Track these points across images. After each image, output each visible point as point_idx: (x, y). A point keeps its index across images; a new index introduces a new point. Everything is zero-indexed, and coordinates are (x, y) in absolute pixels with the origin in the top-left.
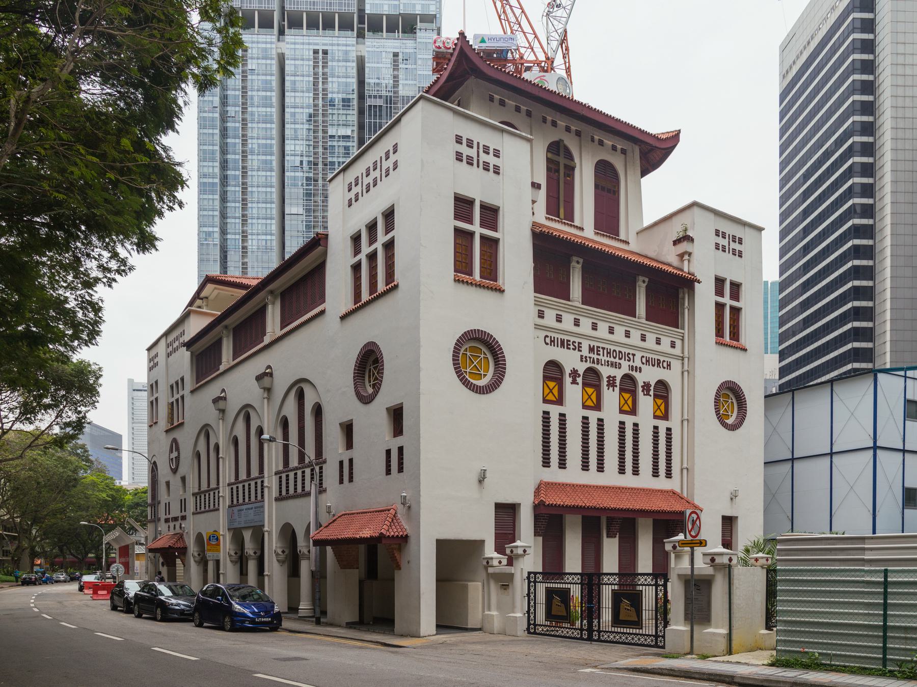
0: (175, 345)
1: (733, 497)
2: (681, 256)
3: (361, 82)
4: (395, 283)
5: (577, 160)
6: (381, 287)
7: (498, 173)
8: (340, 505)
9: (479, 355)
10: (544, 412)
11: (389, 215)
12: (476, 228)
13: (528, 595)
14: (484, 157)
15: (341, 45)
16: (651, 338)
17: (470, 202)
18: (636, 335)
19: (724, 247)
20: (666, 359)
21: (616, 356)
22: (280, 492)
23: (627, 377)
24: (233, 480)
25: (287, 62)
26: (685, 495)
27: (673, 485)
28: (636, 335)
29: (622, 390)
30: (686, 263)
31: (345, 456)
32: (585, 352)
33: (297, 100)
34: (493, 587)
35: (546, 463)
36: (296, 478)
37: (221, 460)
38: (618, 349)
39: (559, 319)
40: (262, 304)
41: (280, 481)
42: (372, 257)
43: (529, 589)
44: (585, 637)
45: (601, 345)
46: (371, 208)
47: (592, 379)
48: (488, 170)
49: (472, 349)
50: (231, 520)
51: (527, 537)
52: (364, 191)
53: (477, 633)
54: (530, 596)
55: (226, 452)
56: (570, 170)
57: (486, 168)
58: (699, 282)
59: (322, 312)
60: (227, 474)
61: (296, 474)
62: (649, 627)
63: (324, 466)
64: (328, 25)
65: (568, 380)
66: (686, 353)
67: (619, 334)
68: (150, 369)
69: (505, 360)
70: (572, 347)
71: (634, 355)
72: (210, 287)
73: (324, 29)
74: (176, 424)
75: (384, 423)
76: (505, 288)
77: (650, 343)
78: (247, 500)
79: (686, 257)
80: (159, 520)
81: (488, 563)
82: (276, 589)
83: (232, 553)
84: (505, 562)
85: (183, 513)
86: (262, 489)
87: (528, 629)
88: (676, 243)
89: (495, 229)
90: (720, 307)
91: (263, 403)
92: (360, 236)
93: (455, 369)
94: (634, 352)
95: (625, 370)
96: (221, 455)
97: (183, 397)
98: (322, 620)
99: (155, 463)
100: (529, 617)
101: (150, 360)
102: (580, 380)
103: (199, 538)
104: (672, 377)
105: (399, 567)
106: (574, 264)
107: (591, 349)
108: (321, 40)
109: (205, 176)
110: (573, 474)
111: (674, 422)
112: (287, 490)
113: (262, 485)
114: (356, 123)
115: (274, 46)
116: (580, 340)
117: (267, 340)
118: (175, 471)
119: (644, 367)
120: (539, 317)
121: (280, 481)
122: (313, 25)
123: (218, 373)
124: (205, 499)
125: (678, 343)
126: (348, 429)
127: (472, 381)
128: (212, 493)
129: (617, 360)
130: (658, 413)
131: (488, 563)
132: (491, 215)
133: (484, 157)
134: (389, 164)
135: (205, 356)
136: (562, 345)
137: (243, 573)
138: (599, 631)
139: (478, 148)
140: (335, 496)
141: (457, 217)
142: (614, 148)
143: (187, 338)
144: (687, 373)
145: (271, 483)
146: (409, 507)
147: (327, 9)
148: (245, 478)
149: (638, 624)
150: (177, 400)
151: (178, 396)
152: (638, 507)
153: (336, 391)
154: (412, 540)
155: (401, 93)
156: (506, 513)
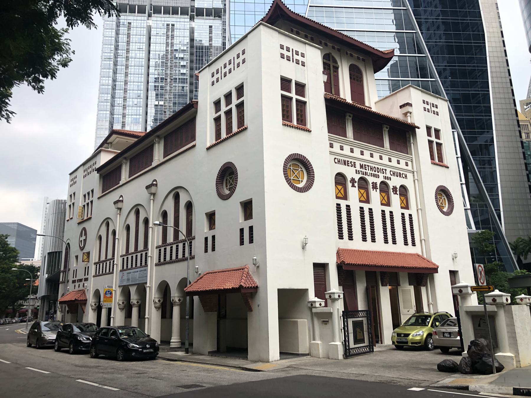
0: (89, 171)
1: (454, 258)
2: (405, 114)
4: (245, 126)
5: (339, 63)
6: (235, 129)
7: (304, 66)
8: (212, 266)
9: (298, 167)
10: (337, 204)
11: (240, 89)
12: (293, 95)
13: (344, 328)
15: (182, 23)
17: (290, 81)
18: (385, 158)
19: (428, 109)
20: (404, 173)
21: (377, 171)
24: (124, 253)
25: (152, 29)
26: (425, 256)
27: (416, 250)
28: (385, 158)
30: (409, 118)
32: (358, 168)
35: (341, 237)
36: (141, 257)
37: (117, 241)
38: (376, 166)
39: (342, 148)
40: (152, 143)
41: (123, 261)
42: (228, 113)
46: (229, 84)
47: (363, 184)
48: (299, 64)
50: (122, 280)
51: (334, 287)
53: (305, 357)
55: (121, 236)
56: (336, 68)
57: (297, 62)
58: (418, 128)
59: (194, 146)
60: (121, 249)
63: (193, 241)
66: (415, 169)
67: (376, 158)
68: (71, 186)
69: (313, 172)
70: (350, 165)
71: (386, 170)
72: (114, 136)
74: (85, 218)
77: (394, 163)
79: (409, 114)
80: (68, 281)
81: (312, 305)
82: (153, 329)
83: (121, 303)
84: (323, 304)
85: (86, 277)
89: (303, 96)
90: (430, 142)
91: (150, 202)
92: (231, 93)
93: (285, 177)
94: (386, 168)
95: (381, 179)
96: (117, 237)
97: (92, 202)
98: (189, 350)
99: (68, 244)
102: (356, 185)
103: (97, 294)
104: (408, 183)
105: (251, 310)
106: (347, 117)
107: (361, 166)
108: (171, 19)
110: (357, 244)
112: (106, 271)
113: (146, 256)
114: (189, 59)
115: (145, 22)
116: (355, 161)
117: (154, 164)
118: (82, 249)
119: (392, 177)
120: (330, 147)
121: (123, 261)
122: (167, 11)
123: (118, 185)
124: (104, 267)
126: (211, 217)
127: (296, 185)
128: (108, 262)
129: (376, 173)
130: (403, 205)
131: (312, 305)
132: (301, 88)
134: (240, 60)
136: (345, 164)
137: (129, 315)
139: (293, 52)
140: (202, 262)
141: (282, 89)
142: (358, 58)
143: (98, 166)
145: (153, 254)
146: (258, 267)
147: (174, 5)
148: (142, 249)
150: (88, 204)
152: (400, 265)
153: (203, 193)
154: (261, 290)
155: (213, 45)
156: (320, 269)
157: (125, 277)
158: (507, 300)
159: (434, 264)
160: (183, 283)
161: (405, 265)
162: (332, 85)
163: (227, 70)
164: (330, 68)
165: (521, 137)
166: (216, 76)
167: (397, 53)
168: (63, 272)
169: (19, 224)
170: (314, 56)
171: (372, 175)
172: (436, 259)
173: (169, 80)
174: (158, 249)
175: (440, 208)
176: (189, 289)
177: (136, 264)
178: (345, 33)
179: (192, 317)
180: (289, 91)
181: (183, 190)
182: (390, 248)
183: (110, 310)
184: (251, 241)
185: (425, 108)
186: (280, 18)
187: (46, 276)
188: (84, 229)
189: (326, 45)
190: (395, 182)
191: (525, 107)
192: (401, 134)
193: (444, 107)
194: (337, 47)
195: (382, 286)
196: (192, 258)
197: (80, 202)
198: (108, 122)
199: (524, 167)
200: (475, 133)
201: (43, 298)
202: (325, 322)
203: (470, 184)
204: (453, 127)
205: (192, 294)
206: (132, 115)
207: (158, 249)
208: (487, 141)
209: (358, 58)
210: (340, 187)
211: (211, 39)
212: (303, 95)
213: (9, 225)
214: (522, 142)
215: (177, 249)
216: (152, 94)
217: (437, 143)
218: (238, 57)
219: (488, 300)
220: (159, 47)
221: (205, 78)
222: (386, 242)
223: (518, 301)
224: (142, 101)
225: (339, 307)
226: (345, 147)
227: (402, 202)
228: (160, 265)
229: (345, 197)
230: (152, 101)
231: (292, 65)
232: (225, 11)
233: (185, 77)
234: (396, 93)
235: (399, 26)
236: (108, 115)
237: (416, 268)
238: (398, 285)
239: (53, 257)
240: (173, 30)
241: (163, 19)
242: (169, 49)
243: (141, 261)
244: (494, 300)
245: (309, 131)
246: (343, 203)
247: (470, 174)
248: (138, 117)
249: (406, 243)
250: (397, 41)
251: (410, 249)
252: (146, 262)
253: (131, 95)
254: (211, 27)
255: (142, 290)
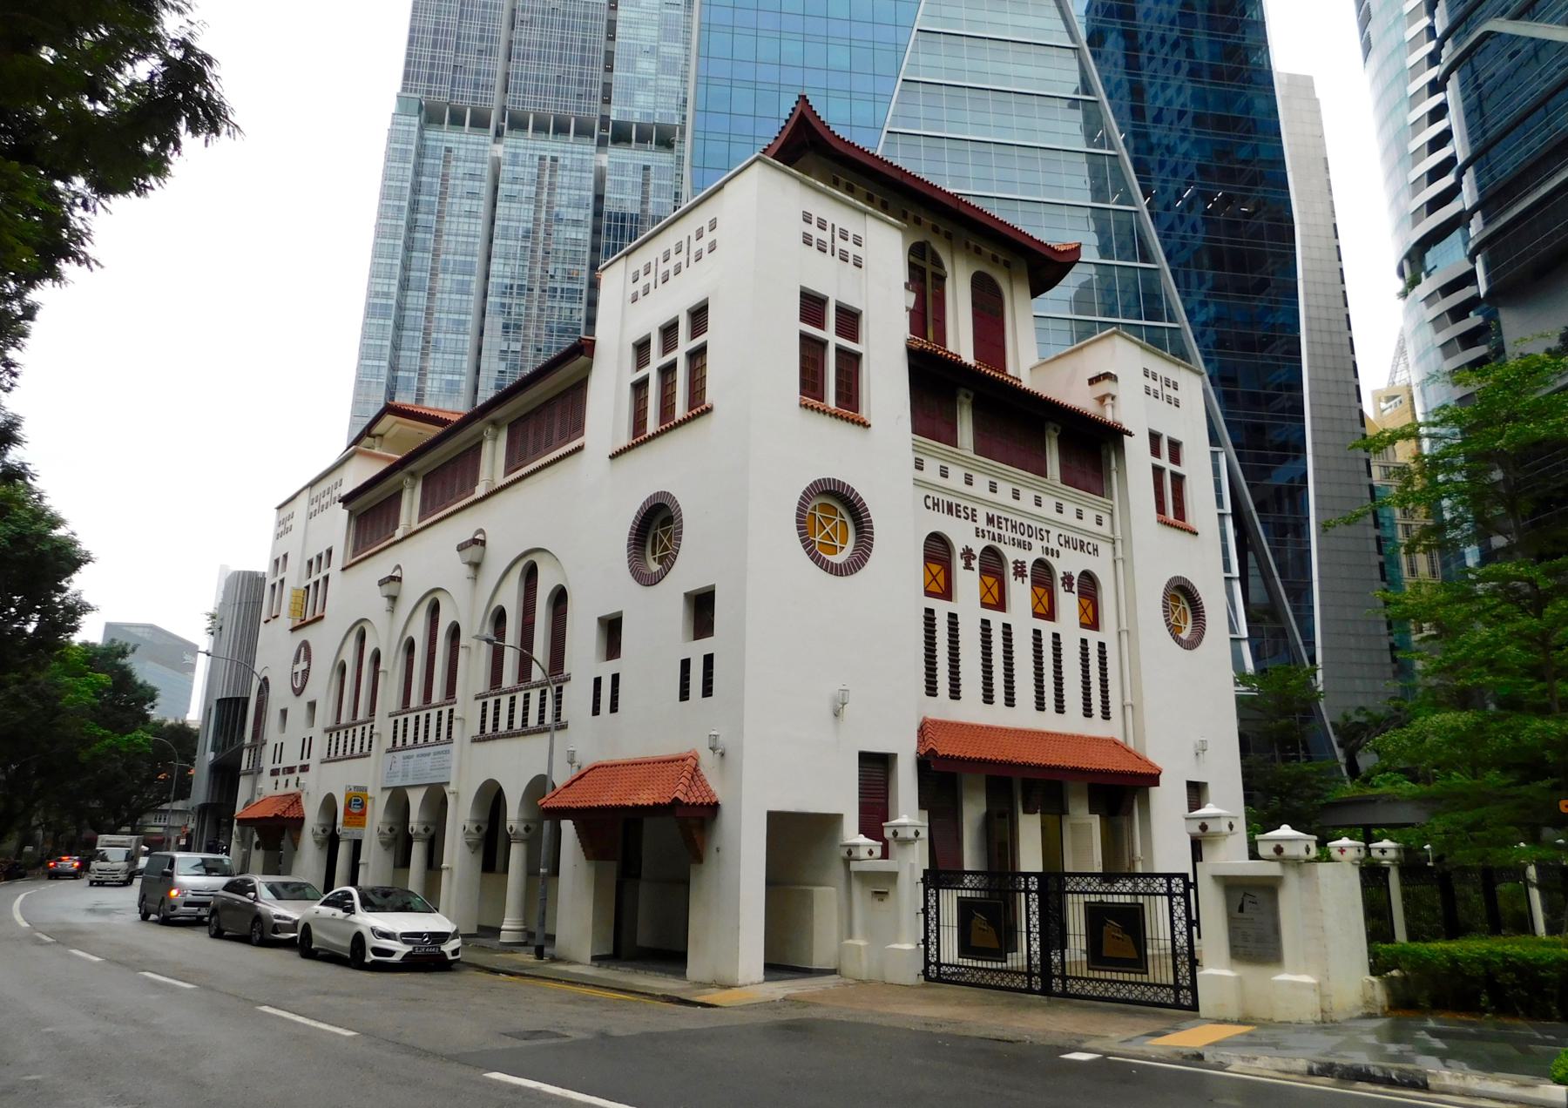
0: (324, 501)
1: (1201, 750)
2: (1101, 400)
3: (599, 198)
6: (680, 411)
9: (834, 518)
11: (699, 316)
12: (830, 335)
14: (840, 244)
15: (571, 150)
16: (1070, 509)
18: (1049, 503)
19: (1156, 392)
21: (1026, 533)
22: (483, 728)
23: (1040, 563)
26: (1131, 745)
27: (1110, 730)
28: (1049, 503)
29: (1035, 583)
30: (1109, 409)
31: (606, 670)
32: (982, 523)
33: (513, 212)
34: (859, 894)
35: (931, 690)
38: (1026, 522)
41: (484, 710)
42: (668, 371)
43: (926, 901)
44: (1038, 988)
45: (1004, 515)
46: (673, 303)
47: (992, 564)
49: (824, 507)
51: (907, 813)
52: (660, 281)
54: (929, 913)
56: (940, 279)
57: (844, 257)
58: (1130, 434)
59: (580, 449)
61: (513, 699)
62: (1161, 972)
63: (566, 687)
64: (561, 129)
65: (959, 563)
68: (279, 536)
72: (389, 419)
73: (555, 133)
74: (308, 618)
75: (677, 615)
76: (872, 422)
77: (1069, 516)
78: (421, 739)
79: (1108, 401)
80: (260, 771)
84: (878, 852)
85: (305, 762)
86: (450, 723)
87: (925, 972)
88: (1092, 381)
89: (855, 339)
90: (1158, 472)
95: (1037, 553)
96: (381, 668)
97: (326, 578)
99: (265, 679)
100: (927, 949)
101: (280, 523)
102: (975, 564)
106: (961, 398)
107: (990, 520)
108: (550, 146)
109: (377, 295)
110: (971, 710)
111: (1107, 634)
113: (451, 717)
118: (298, 692)
119: (1062, 550)
121: (484, 710)
125: (1106, 519)
126: (612, 628)
127: (829, 557)
128: (359, 729)
129: (1025, 538)
131: (850, 853)
132: (849, 321)
133: (840, 244)
135: (371, 513)
136: (950, 511)
137: (403, 862)
138: (1064, 978)
141: (804, 317)
143: (346, 490)
144: (1121, 562)
146: (722, 755)
149: (1139, 962)
150: (317, 583)
151: (320, 577)
152: (1071, 763)
156: (876, 768)
157: (398, 767)
158: (1308, 850)
159: (1151, 765)
160: (539, 786)
161: (1084, 764)
162: (927, 314)
163: (670, 266)
164: (925, 279)
165: (1370, 475)
166: (643, 281)
167: (1090, 254)
168: (250, 748)
169: (152, 628)
170: (885, 246)
171: (1014, 542)
172: (1157, 752)
173: (537, 292)
174: (480, 702)
175: (1174, 631)
176: (549, 801)
177: (426, 737)
178: (972, 201)
179: (555, 871)
180: (821, 324)
181: (546, 555)
182: (1049, 722)
183: (357, 846)
184: (707, 691)
185: (1147, 388)
186: (807, 147)
187: (211, 756)
188: (305, 645)
189: (917, 221)
190: (1068, 563)
191: (1383, 405)
192: (1090, 446)
193: (1193, 388)
194: (940, 224)
195: (1026, 812)
196: (564, 727)
197: (295, 577)
198: (384, 387)
199: (1373, 546)
200: (1264, 458)
201: (203, 810)
202: (881, 895)
203: (1251, 580)
204: (1214, 439)
205: (557, 814)
206: (442, 373)
207: (480, 702)
208: (1292, 480)
209: (995, 259)
210: (935, 568)
211: (644, 201)
212: (854, 338)
213: (133, 630)
214: (1372, 488)
215: (526, 703)
216: (494, 323)
217: (1173, 474)
218: (700, 235)
219: (1265, 850)
220: (515, 215)
221: (614, 281)
222: (1040, 706)
223: (1335, 853)
224: (469, 342)
225: (914, 861)
226: (952, 470)
227: (1083, 611)
228: (484, 740)
229: (947, 594)
230: (494, 340)
231: (830, 262)
232: (683, 133)
233: (578, 287)
234: (1081, 348)
235: (1098, 192)
236: (385, 372)
237: (1107, 773)
238: (1063, 811)
239: (230, 712)
240: (553, 171)
241: (530, 144)
242: (543, 216)
243: (439, 730)
244: (1279, 850)
245: (866, 425)
246: (942, 608)
247: (1251, 556)
248: (456, 378)
249: (1088, 712)
250: (1092, 227)
251: (1096, 728)
252: (449, 733)
253: (444, 324)
254: (646, 168)
255: (437, 800)
